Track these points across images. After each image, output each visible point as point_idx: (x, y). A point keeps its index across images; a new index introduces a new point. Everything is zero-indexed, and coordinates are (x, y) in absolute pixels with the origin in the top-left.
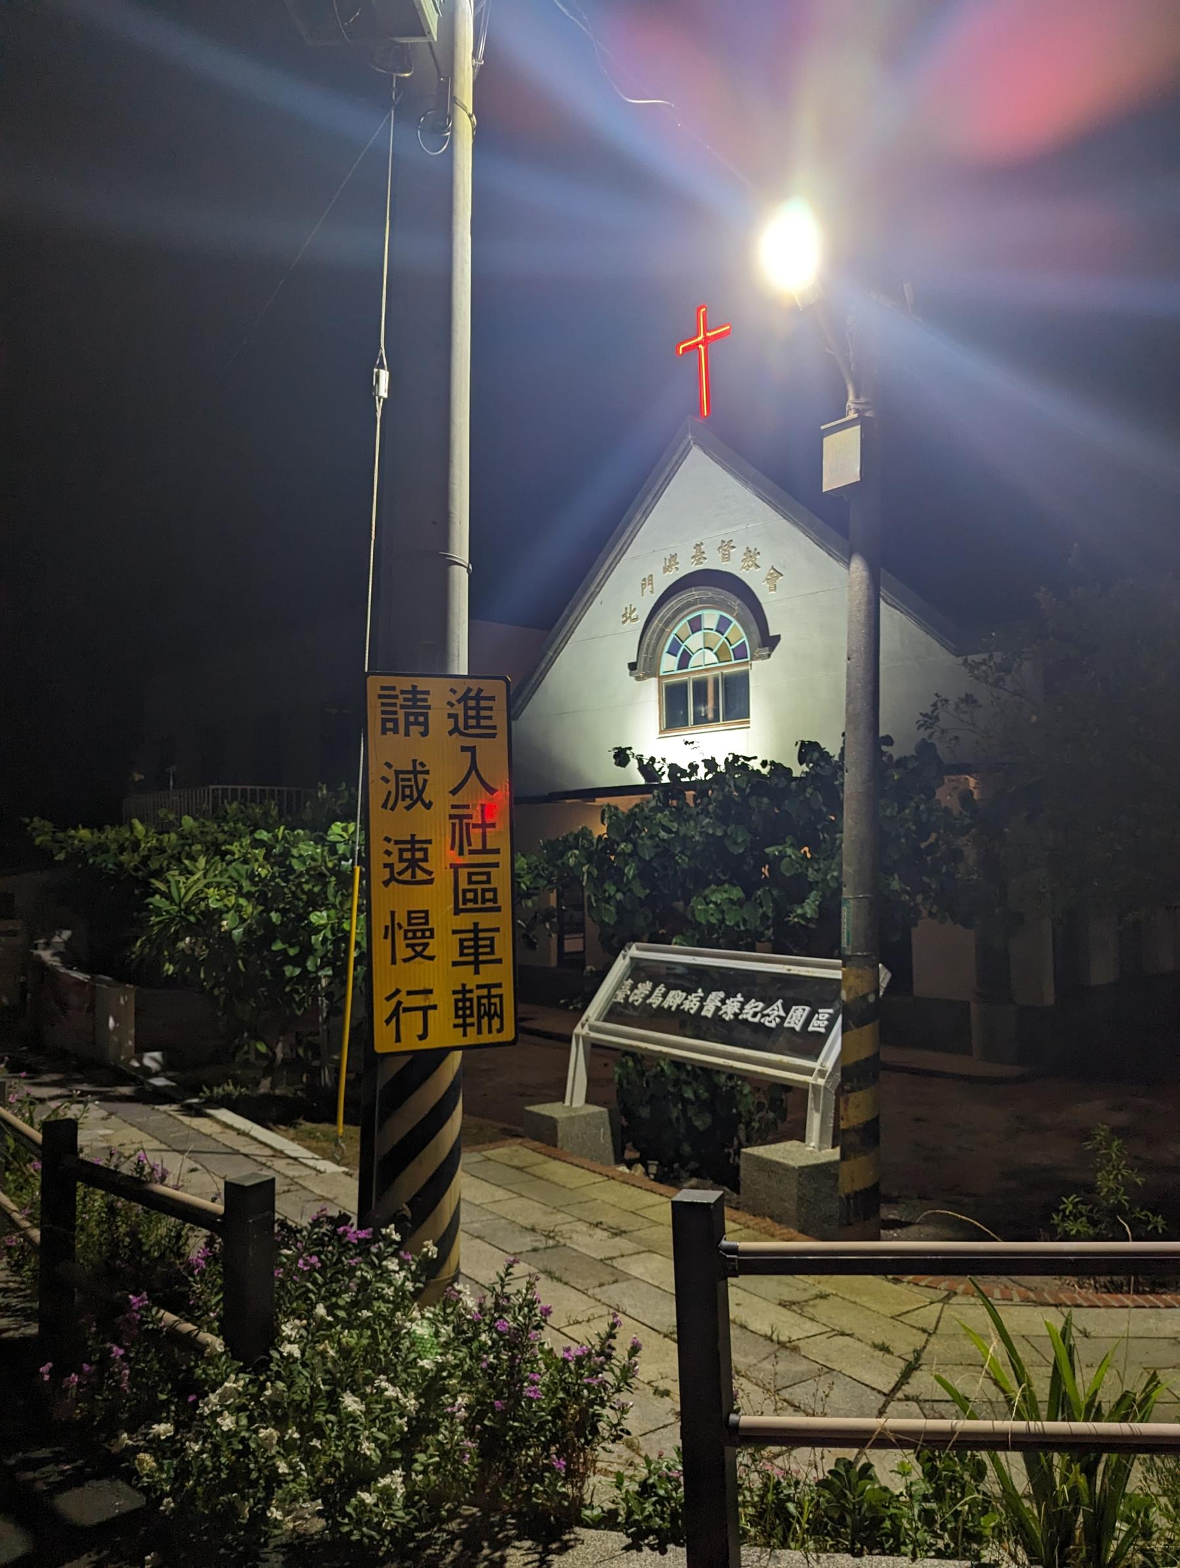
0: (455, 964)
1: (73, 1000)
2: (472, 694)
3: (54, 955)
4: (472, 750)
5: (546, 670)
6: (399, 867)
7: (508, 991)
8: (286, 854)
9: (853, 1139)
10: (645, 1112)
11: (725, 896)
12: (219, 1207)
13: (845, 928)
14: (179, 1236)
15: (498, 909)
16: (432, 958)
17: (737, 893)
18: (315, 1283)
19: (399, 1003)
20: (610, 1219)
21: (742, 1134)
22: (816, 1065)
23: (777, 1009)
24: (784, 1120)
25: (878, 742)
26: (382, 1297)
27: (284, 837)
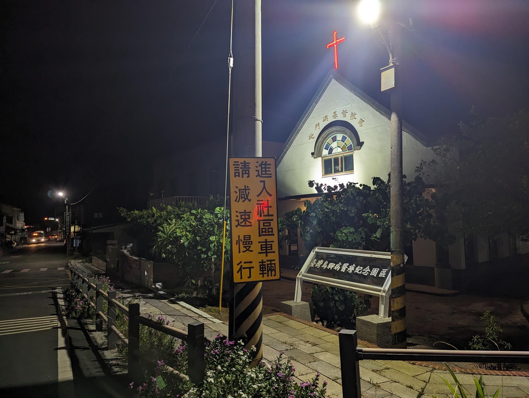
0: (259, 253)
1: (134, 266)
2: (264, 163)
3: (127, 251)
4: (264, 182)
5: (283, 156)
6: (241, 221)
7: (277, 262)
8: (201, 218)
9: (396, 314)
10: (322, 304)
11: (348, 231)
12: (186, 333)
13: (391, 241)
14: (172, 342)
15: (273, 235)
16: (252, 251)
17: (352, 230)
18: (216, 358)
19: (242, 266)
20: (311, 340)
21: (355, 312)
22: (382, 289)
23: (368, 269)
24: (370, 308)
25: (402, 176)
26: (238, 364)
27: (201, 212)
